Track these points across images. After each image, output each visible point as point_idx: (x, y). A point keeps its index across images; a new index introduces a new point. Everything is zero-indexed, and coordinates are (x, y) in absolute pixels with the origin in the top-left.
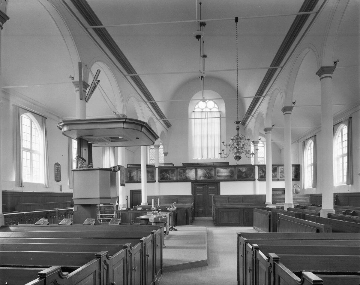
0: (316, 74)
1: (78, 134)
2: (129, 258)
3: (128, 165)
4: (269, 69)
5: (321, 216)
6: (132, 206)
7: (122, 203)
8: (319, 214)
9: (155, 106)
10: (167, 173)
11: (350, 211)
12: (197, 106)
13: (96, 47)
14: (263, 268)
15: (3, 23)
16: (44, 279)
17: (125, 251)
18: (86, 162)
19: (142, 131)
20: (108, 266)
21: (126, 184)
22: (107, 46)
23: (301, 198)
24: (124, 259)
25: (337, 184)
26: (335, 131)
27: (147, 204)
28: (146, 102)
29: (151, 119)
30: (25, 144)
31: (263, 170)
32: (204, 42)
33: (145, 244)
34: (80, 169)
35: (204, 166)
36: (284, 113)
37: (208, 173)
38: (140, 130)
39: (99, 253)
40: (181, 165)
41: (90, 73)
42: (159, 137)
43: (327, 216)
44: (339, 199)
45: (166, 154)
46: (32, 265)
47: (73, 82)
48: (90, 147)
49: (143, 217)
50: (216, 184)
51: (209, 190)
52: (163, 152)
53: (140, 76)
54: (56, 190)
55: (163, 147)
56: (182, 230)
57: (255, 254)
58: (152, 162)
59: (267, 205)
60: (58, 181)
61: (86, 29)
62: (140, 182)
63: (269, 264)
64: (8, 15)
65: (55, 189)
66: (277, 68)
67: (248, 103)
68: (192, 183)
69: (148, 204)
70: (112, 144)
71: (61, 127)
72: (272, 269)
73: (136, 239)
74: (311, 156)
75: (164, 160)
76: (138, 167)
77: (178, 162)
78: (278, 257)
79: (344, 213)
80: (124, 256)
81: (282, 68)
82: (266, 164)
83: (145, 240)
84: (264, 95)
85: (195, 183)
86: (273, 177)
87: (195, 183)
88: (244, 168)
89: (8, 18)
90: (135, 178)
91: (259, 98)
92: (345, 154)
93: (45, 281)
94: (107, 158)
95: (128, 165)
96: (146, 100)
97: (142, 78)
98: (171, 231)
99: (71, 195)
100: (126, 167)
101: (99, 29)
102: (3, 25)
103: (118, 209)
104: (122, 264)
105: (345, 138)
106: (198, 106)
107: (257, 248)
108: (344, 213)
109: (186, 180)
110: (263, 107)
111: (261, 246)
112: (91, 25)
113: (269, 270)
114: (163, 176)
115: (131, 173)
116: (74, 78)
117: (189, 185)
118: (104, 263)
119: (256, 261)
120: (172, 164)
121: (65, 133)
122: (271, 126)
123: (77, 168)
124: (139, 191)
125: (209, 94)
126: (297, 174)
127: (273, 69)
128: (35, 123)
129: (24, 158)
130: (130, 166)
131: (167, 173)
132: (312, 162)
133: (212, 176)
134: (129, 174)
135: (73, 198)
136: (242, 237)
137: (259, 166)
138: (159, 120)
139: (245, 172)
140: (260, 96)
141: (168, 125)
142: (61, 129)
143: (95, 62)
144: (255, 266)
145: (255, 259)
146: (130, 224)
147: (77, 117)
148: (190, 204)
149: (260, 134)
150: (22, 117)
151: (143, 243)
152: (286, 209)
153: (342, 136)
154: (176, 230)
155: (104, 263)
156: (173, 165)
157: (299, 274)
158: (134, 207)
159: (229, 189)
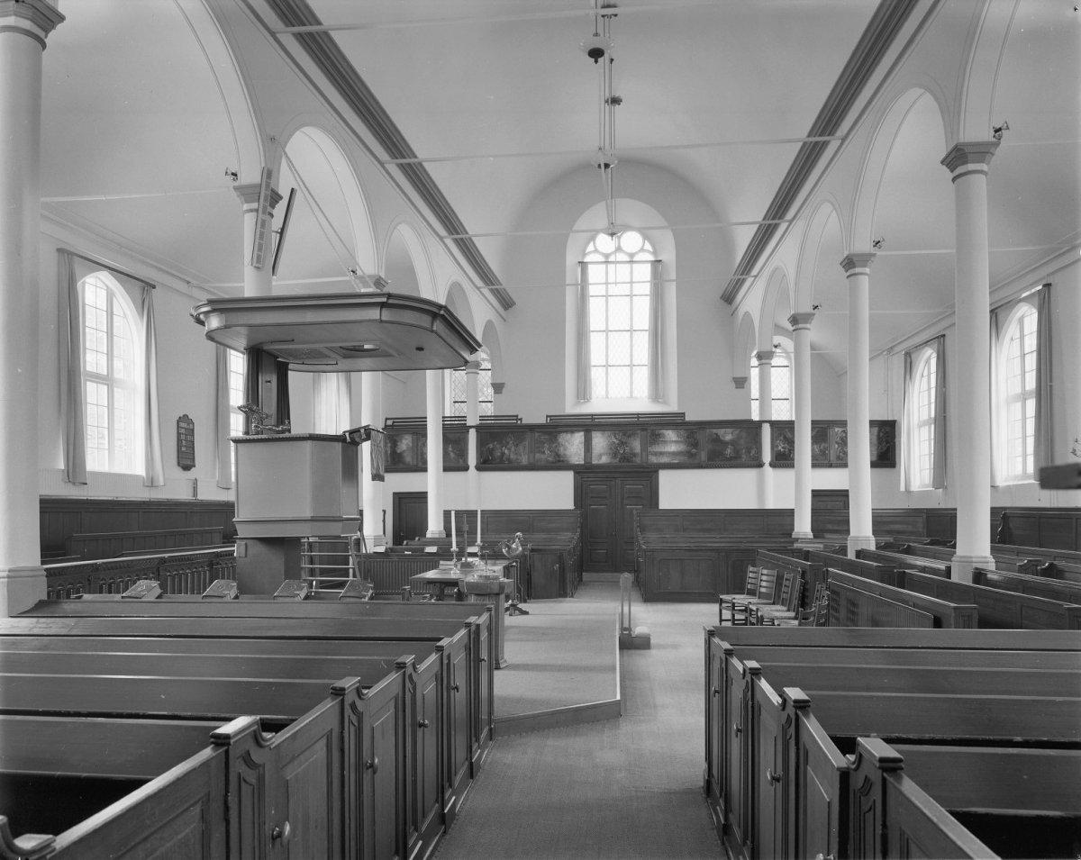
0: (942, 162)
1: (249, 339)
2: (410, 694)
4: (805, 144)
5: (955, 578)
6: (398, 539)
7: (374, 531)
8: (948, 572)
9: (468, 250)
10: (501, 443)
11: (1039, 563)
12: (591, 248)
13: (300, 81)
14: (770, 728)
15: (47, 31)
16: (225, 748)
17: (401, 677)
18: (272, 419)
19: (435, 329)
20: (360, 716)
21: (388, 476)
22: (331, 81)
23: (898, 519)
24: (396, 699)
25: (1005, 481)
26: (1000, 325)
28: (441, 238)
29: (455, 289)
30: (93, 360)
31: (785, 437)
32: (612, 60)
33: (449, 657)
34: (256, 437)
35: (612, 425)
36: (848, 274)
37: (622, 443)
38: (431, 332)
39: (339, 684)
40: (542, 421)
41: (284, 160)
42: (480, 346)
43: (970, 577)
44: (1010, 526)
45: (498, 388)
46: (166, 713)
47: (236, 188)
48: (282, 373)
49: (431, 574)
50: (648, 475)
51: (626, 496)
52: (490, 382)
54: (182, 493)
55: (490, 368)
56: (541, 613)
57: (752, 688)
58: (462, 410)
59: (797, 540)
60: (187, 468)
61: (273, 34)
62: (425, 470)
63: (784, 716)
64: (61, 9)
65: (176, 488)
66: (829, 142)
67: (743, 238)
68: (576, 473)
70: (344, 364)
71: (202, 317)
72: (792, 730)
73: (429, 641)
74: (929, 396)
75: (495, 405)
76: (418, 429)
77: (534, 415)
78: (807, 698)
79: (1023, 569)
80: (397, 689)
81: (844, 140)
82: (794, 419)
83: (450, 645)
84: (790, 215)
85: (585, 473)
86: (814, 457)
87: (585, 473)
88: (729, 430)
89: (62, 18)
90: (408, 459)
91: (776, 226)
92: (1031, 391)
93: (227, 752)
94: (330, 403)
95: (387, 419)
96: (443, 232)
98: (511, 615)
99: (227, 509)
100: (380, 426)
101: (311, 34)
102: (46, 37)
103: (359, 550)
104: (392, 710)
105: (1031, 343)
106: (595, 246)
107: (755, 673)
108: (1023, 569)
109: (559, 464)
110: (784, 253)
111: (768, 667)
113: (785, 731)
114: (491, 452)
115: (400, 443)
116: (239, 175)
117: (566, 480)
118: (350, 711)
119: (753, 707)
120: (517, 416)
121: (213, 335)
122: (810, 310)
123: (247, 433)
124: (422, 497)
125: (629, 209)
126: (888, 448)
127: (817, 143)
128: (121, 300)
129: (89, 400)
130: (394, 422)
131: (501, 443)
132: (933, 415)
133: (635, 455)
134: (391, 447)
135: (234, 520)
136: (716, 640)
137: (773, 424)
138: (478, 288)
139: (733, 443)
140: (779, 218)
141: (506, 303)
142: (202, 323)
143: (297, 129)
144: (750, 720)
145: (750, 703)
146: (403, 599)
147: (249, 287)
148: (569, 534)
149: (779, 329)
150: (84, 283)
151: (445, 654)
152: (851, 556)
153: (1022, 337)
154: (526, 613)
156: (521, 419)
157: (846, 745)
158: (405, 542)
159: (682, 490)
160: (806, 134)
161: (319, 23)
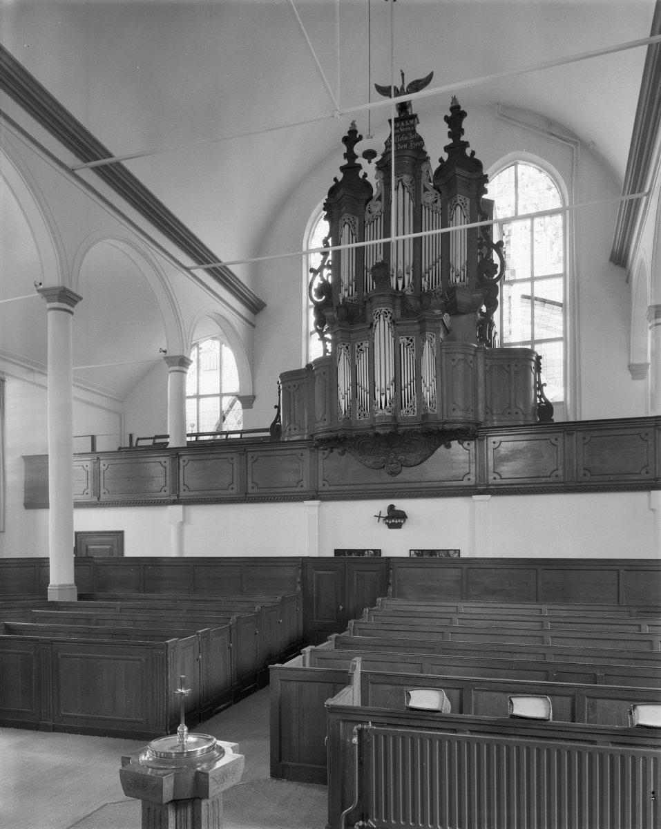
3: (410, 550)
4: (650, 47)
27: (75, 599)
43: (76, 598)
47: (165, 358)
53: (124, 163)
69: (81, 597)
97: (137, 169)
101: (105, 166)
112: (86, 160)
138: (187, 269)
140: (639, 192)
152: (457, 623)
155: (234, 786)
160: (649, 36)
161: (110, 156)
